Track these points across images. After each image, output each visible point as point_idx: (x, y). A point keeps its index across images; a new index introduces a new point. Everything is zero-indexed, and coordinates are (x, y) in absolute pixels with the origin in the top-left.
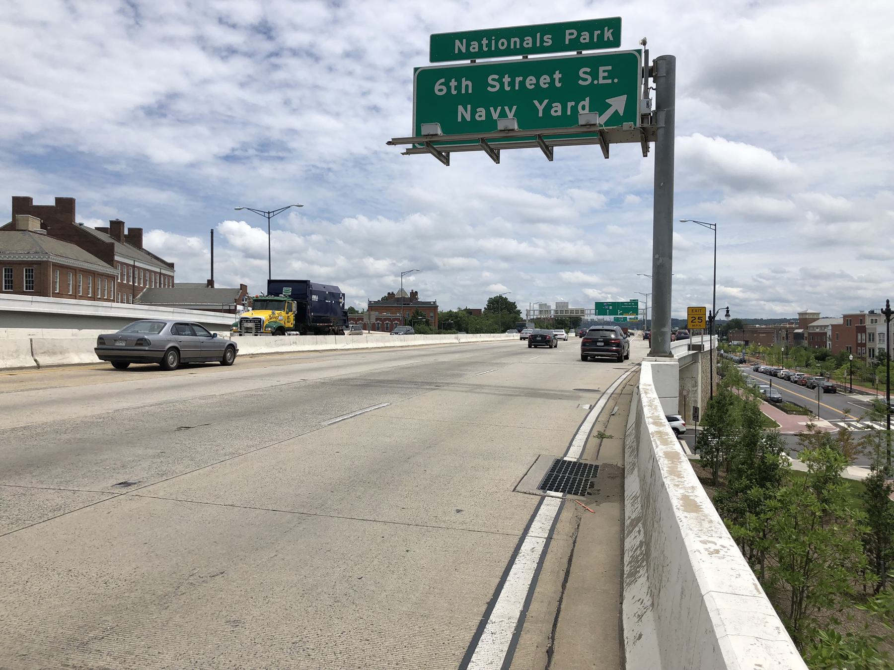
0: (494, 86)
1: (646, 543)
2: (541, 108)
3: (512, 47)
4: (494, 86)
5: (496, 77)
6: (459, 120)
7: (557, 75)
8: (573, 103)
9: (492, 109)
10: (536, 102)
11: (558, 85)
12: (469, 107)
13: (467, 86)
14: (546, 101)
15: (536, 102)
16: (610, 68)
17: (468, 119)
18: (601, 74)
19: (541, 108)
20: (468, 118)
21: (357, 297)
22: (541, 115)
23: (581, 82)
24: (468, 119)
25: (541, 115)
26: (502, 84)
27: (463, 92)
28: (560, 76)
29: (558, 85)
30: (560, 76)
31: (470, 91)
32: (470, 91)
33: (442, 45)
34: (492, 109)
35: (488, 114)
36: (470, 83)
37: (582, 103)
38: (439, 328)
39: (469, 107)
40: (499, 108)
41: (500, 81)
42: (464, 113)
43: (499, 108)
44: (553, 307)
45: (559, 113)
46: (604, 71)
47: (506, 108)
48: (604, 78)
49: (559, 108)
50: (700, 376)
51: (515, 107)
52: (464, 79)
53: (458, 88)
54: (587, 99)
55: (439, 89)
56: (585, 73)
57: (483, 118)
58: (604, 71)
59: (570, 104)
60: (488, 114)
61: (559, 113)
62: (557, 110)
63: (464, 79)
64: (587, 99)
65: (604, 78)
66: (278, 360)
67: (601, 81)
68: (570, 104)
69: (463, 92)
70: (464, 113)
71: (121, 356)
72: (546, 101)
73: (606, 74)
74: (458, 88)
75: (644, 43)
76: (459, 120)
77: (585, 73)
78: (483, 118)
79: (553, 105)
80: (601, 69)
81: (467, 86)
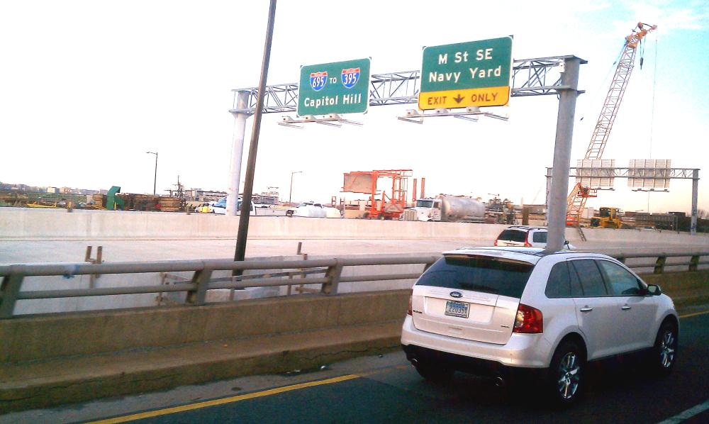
5: (460, 53)
6: (430, 81)
8: (492, 70)
9: (447, 74)
12: (436, 73)
14: (477, 69)
18: (487, 54)
20: (435, 80)
25: (473, 77)
29: (466, 60)
36: (480, 59)
37: (497, 70)
38: (678, 228)
39: (436, 73)
40: (451, 74)
41: (462, 56)
43: (451, 74)
48: (489, 56)
49: (484, 73)
50: (685, 316)
54: (500, 67)
57: (442, 80)
62: (482, 74)
64: (500, 67)
67: (487, 58)
68: (490, 70)
71: (505, 236)
72: (477, 69)
73: (489, 54)
75: (653, 28)
76: (430, 81)
80: (487, 50)
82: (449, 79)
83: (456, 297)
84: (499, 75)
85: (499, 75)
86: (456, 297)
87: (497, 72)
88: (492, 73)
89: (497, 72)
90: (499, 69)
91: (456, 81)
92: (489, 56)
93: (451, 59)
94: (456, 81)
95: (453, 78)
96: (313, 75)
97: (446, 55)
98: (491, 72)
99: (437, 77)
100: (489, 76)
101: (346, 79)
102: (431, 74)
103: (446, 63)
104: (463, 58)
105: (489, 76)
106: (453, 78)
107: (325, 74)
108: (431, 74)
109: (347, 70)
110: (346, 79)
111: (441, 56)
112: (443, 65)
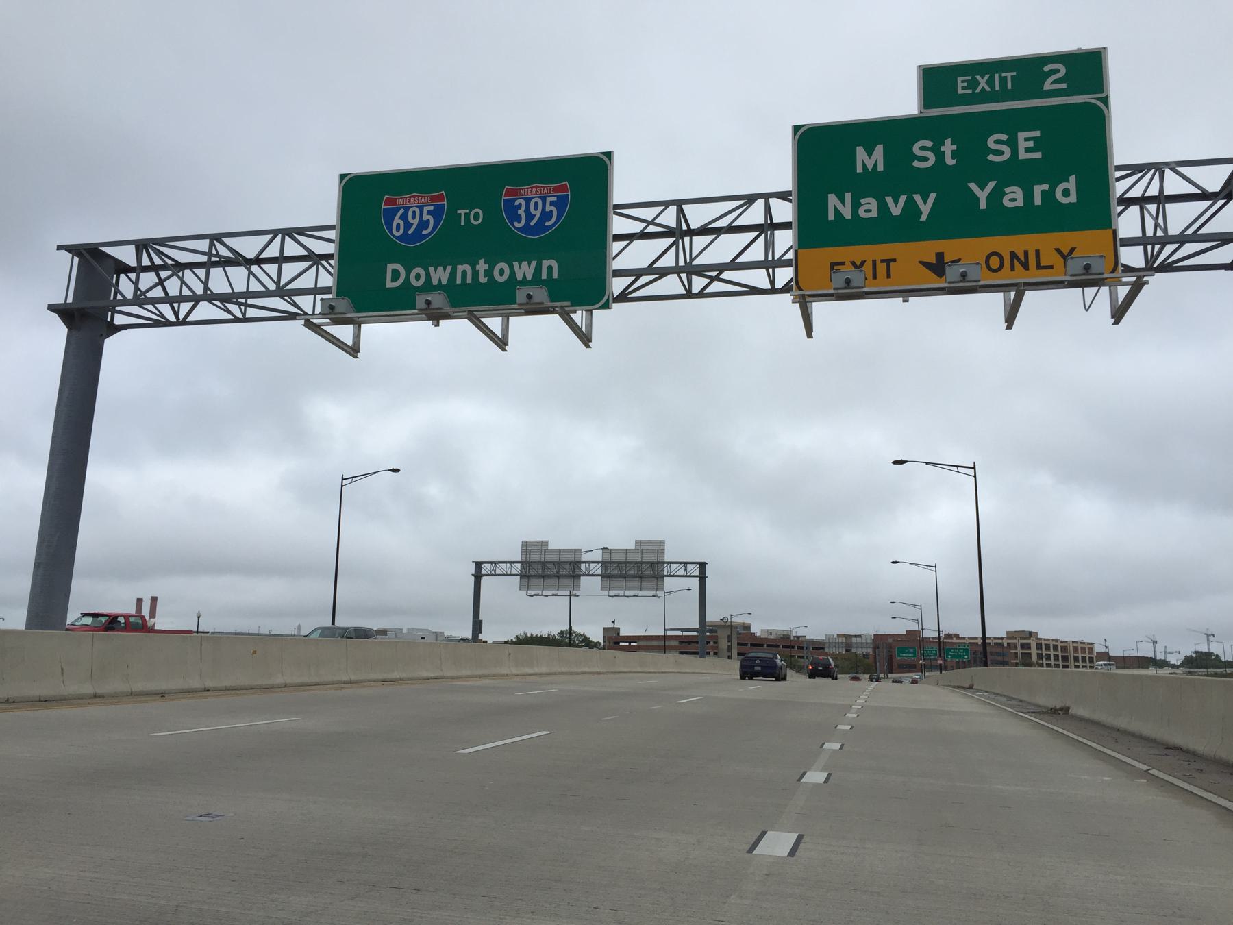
1: (754, 291)
2: (982, 195)
3: (459, 281)
6: (831, 217)
7: (948, 147)
8: (1046, 187)
9: (889, 200)
10: (973, 186)
11: (950, 161)
12: (848, 196)
14: (992, 184)
15: (973, 186)
16: (1037, 134)
18: (1022, 145)
19: (982, 195)
21: (699, 136)
22: (983, 205)
25: (983, 205)
26: (940, 156)
29: (950, 161)
34: (889, 200)
35: (883, 207)
39: (848, 196)
40: (903, 199)
41: (936, 150)
42: (840, 206)
43: (903, 199)
46: (1027, 139)
47: (917, 198)
51: (933, 196)
54: (1073, 178)
55: (1068, 191)
57: (874, 214)
58: (1027, 139)
60: (883, 207)
61: (1020, 203)
64: (1073, 178)
65: (1027, 150)
67: (1022, 155)
70: (840, 206)
72: (992, 184)
73: (1031, 144)
76: (831, 217)
78: (874, 214)
79: (1007, 190)
82: (896, 210)
84: (1073, 198)
85: (1073, 198)
87: (1066, 193)
88: (1048, 196)
89: (1066, 193)
90: (1072, 184)
91: (924, 218)
94: (924, 218)
97: (879, 149)
98: (1043, 192)
99: (856, 206)
100: (1038, 201)
101: (521, 212)
102: (833, 199)
103: (880, 168)
105: (1038, 201)
107: (441, 198)
108: (833, 199)
109: (522, 190)
110: (521, 212)
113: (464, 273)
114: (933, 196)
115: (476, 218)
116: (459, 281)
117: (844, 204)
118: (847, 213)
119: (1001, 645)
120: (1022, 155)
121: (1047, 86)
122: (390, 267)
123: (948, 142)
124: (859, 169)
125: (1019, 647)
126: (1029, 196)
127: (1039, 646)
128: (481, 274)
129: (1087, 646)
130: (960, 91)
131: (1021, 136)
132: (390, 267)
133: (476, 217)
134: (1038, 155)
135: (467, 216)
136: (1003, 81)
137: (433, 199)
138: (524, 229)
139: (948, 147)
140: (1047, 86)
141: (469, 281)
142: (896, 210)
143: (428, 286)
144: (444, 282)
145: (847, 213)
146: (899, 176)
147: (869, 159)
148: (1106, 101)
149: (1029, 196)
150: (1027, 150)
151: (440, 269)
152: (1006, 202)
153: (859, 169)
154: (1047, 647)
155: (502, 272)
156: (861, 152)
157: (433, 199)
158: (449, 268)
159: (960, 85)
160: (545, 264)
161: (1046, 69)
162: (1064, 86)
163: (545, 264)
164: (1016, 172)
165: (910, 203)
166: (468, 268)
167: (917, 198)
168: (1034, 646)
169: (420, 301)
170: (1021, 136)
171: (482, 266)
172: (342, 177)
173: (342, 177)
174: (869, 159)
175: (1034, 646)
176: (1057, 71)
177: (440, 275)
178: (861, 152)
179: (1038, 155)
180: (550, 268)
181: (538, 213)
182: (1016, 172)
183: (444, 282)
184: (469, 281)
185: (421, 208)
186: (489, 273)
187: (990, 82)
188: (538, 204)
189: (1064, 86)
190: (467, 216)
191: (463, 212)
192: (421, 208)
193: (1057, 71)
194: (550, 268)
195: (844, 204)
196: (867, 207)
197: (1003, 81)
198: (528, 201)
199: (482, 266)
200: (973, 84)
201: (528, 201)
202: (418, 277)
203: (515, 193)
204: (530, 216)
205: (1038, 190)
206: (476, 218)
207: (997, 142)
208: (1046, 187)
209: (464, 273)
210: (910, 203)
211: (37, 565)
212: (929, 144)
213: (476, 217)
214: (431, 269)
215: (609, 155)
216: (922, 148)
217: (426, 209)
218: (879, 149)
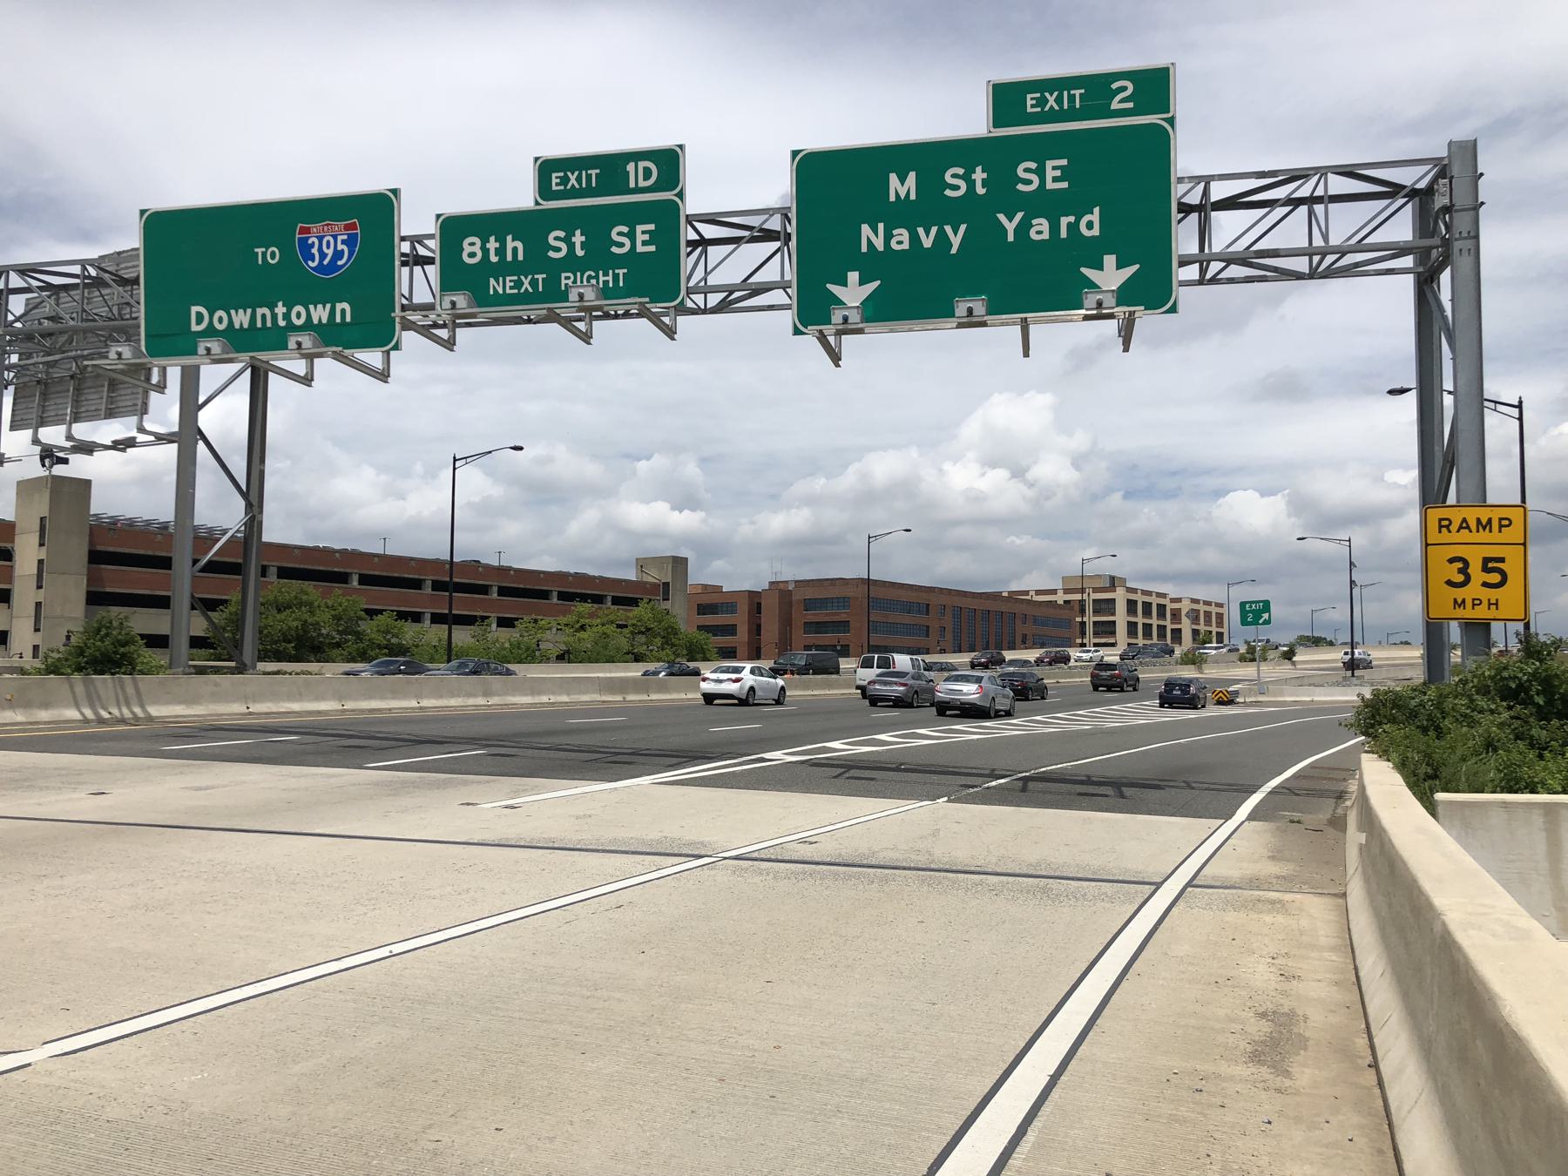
0: (558, 250)
2: (1010, 227)
3: (338, 320)
4: (558, 250)
6: (864, 249)
7: (979, 175)
8: (1072, 219)
9: (921, 231)
10: (1001, 217)
11: (980, 190)
12: (881, 226)
13: (515, 250)
14: (1019, 215)
15: (1001, 217)
16: (1064, 162)
17: (881, 248)
18: (640, 238)
19: (1010, 227)
22: (1011, 238)
23: (1021, 187)
24: (881, 248)
25: (1011, 238)
26: (971, 184)
27: (509, 258)
28: (985, 175)
29: (980, 190)
30: (985, 175)
31: (520, 257)
32: (520, 257)
33: (546, 168)
34: (921, 231)
35: (914, 239)
36: (519, 245)
39: (881, 226)
40: (934, 230)
41: (967, 177)
43: (934, 230)
44: (1293, 519)
45: (1046, 236)
46: (1054, 168)
47: (948, 229)
48: (644, 243)
51: (963, 227)
52: (509, 238)
53: (501, 251)
54: (1097, 210)
55: (471, 249)
56: (556, 238)
57: (906, 246)
58: (1054, 168)
59: (1065, 221)
60: (914, 239)
61: (1046, 236)
63: (509, 238)
64: (1097, 210)
65: (1055, 179)
66: (351, 737)
67: (1050, 185)
68: (1065, 221)
69: (509, 258)
72: (1019, 215)
74: (501, 251)
76: (864, 249)
77: (556, 238)
78: (906, 246)
79: (1034, 222)
81: (515, 250)
82: (927, 243)
83: (971, 712)
84: (1096, 232)
85: (1096, 232)
86: (971, 712)
87: (1090, 225)
88: (1073, 228)
89: (1090, 225)
90: (1095, 216)
91: (954, 251)
92: (644, 243)
93: (931, 184)
94: (954, 251)
95: (942, 238)
96: (308, 231)
97: (912, 176)
98: (1069, 224)
99: (888, 237)
100: (1064, 234)
101: (315, 251)
102: (866, 229)
103: (913, 197)
104: (571, 246)
105: (1064, 234)
106: (942, 238)
107: (353, 227)
108: (866, 229)
109: (314, 227)
110: (315, 251)
111: (893, 178)
112: (903, 202)
113: (264, 316)
114: (963, 227)
115: (273, 257)
116: (338, 320)
117: (869, 240)
118: (879, 244)
119: (1052, 604)
120: (1050, 185)
121: (1115, 105)
122: (194, 309)
123: (979, 169)
124: (892, 198)
125: (1089, 608)
126: (1055, 228)
127: (1131, 604)
128: (280, 317)
129: (1214, 610)
130: (1029, 110)
131: (1049, 164)
132: (194, 309)
133: (273, 255)
134: (1065, 185)
135: (264, 254)
136: (1072, 98)
137: (347, 227)
138: (318, 269)
139: (979, 175)
140: (1115, 105)
141: (269, 324)
142: (927, 243)
143: (211, 332)
144: (324, 321)
145: (879, 244)
146: (931, 207)
147: (902, 187)
148: (1171, 121)
149: (1055, 228)
150: (1055, 179)
151: (320, 306)
152: (1033, 236)
153: (892, 198)
154: (1147, 607)
155: (299, 316)
156: (893, 179)
157: (347, 227)
158: (328, 306)
159: (1029, 103)
160: (339, 306)
161: (1114, 86)
162: (1131, 105)
163: (339, 306)
164: (1044, 204)
165: (941, 235)
166: (266, 311)
167: (948, 229)
168: (1121, 607)
169: (292, 344)
170: (1049, 164)
171: (280, 309)
172: (795, 153)
173: (795, 153)
174: (902, 187)
175: (1121, 607)
176: (1124, 89)
177: (320, 314)
178: (893, 179)
179: (1065, 185)
180: (343, 311)
181: (330, 252)
182: (1044, 204)
183: (324, 321)
184: (269, 324)
185: (335, 237)
186: (287, 316)
187: (1059, 100)
188: (329, 243)
189: (1131, 105)
190: (264, 254)
191: (259, 251)
192: (335, 237)
193: (1124, 89)
194: (343, 311)
195: (869, 240)
196: (1039, 228)
197: (1072, 98)
198: (320, 239)
199: (280, 309)
200: (1042, 102)
201: (320, 239)
202: (220, 320)
203: (308, 231)
204: (323, 255)
205: (1064, 221)
206: (273, 257)
207: (1026, 170)
208: (1072, 219)
209: (264, 316)
210: (941, 235)
211: (1415, 881)
212: (961, 171)
213: (273, 255)
214: (311, 307)
215: (395, 192)
216: (954, 176)
217: (340, 238)
218: (912, 176)
